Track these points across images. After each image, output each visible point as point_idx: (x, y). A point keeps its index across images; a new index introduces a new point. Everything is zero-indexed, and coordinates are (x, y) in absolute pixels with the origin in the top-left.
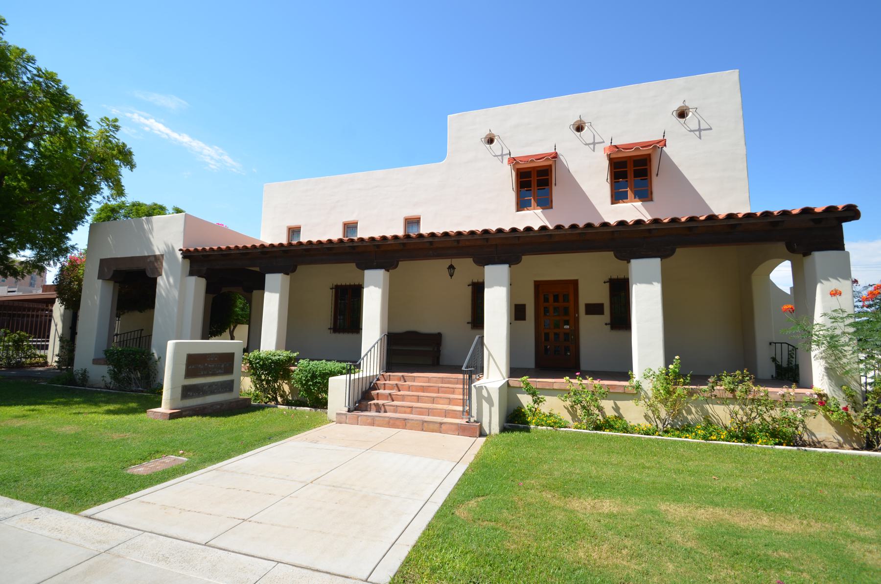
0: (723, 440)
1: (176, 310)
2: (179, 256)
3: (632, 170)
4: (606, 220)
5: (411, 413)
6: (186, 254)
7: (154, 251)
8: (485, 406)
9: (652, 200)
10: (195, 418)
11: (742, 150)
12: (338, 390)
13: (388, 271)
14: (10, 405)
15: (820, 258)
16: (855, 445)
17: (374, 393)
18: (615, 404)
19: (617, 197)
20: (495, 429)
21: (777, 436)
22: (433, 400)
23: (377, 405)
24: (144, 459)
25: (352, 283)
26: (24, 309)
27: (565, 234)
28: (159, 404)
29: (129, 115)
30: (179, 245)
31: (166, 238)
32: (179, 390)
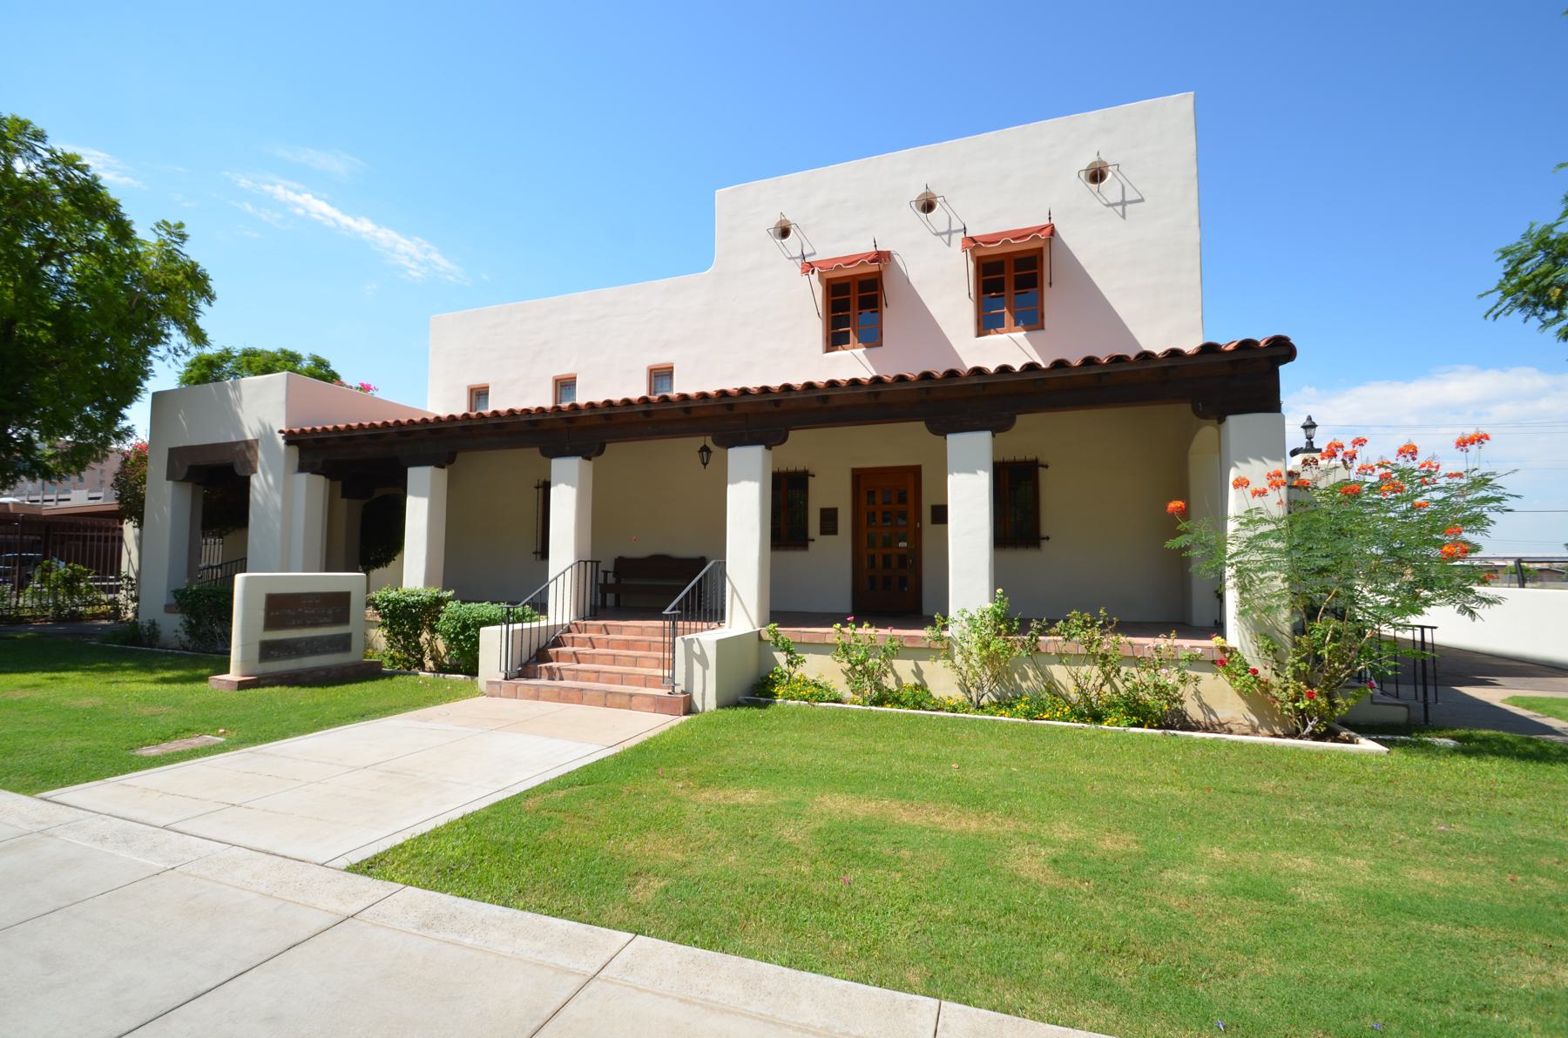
0: (1059, 719)
1: (278, 526)
2: (282, 442)
3: (1013, 276)
4: (1146, 348)
5: (597, 681)
6: (291, 438)
7: (243, 434)
8: (697, 668)
9: (1042, 328)
10: (277, 688)
11: (1193, 235)
12: (492, 644)
13: (769, 447)
14: (24, 672)
15: (1238, 426)
16: (1277, 730)
17: (552, 651)
18: (917, 665)
19: (986, 324)
20: (711, 704)
21: (1139, 714)
22: (635, 662)
23: (550, 669)
24: (165, 739)
25: (792, 468)
26: (85, 528)
27: (1099, 375)
28: (228, 672)
29: (268, 188)
30: (280, 424)
31: (262, 410)
32: (256, 649)
